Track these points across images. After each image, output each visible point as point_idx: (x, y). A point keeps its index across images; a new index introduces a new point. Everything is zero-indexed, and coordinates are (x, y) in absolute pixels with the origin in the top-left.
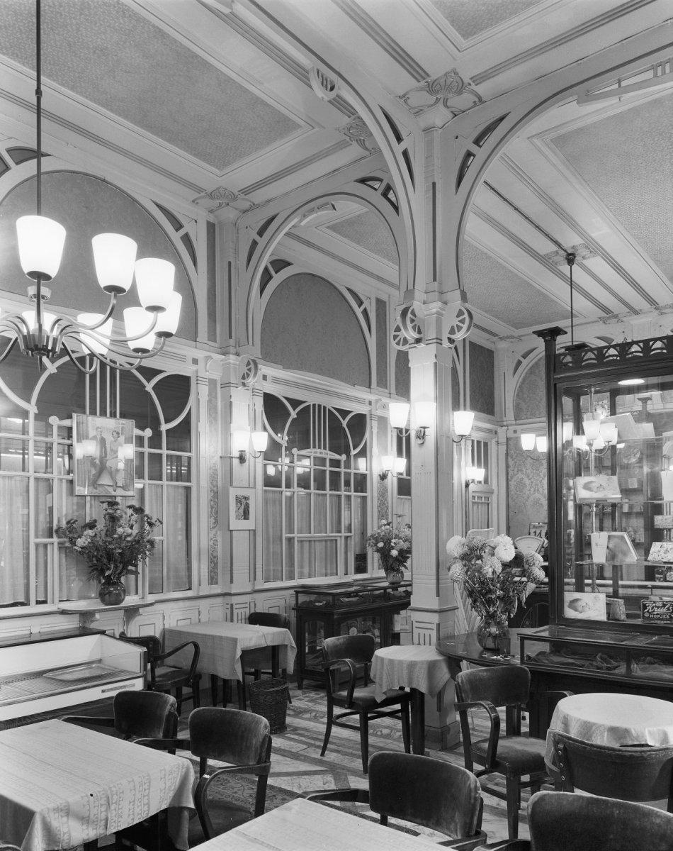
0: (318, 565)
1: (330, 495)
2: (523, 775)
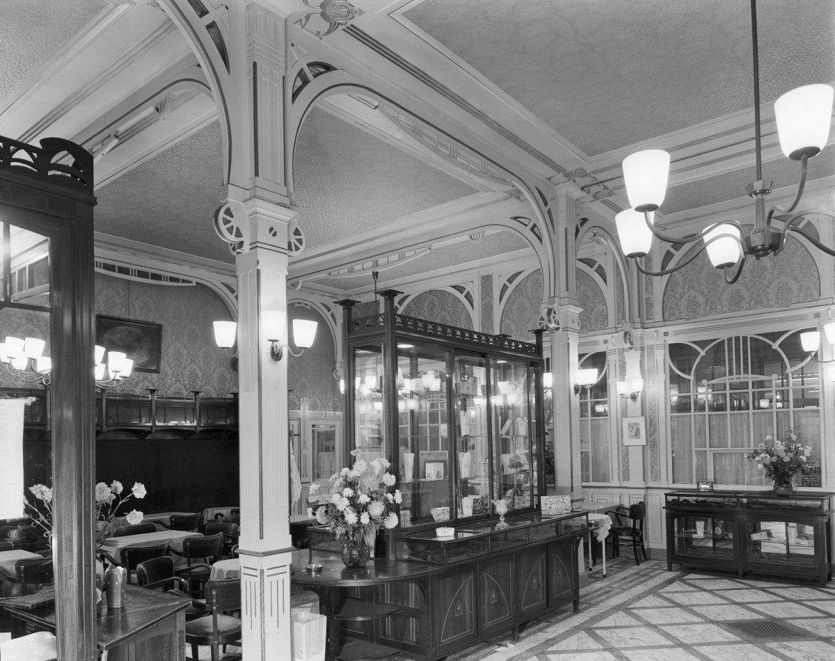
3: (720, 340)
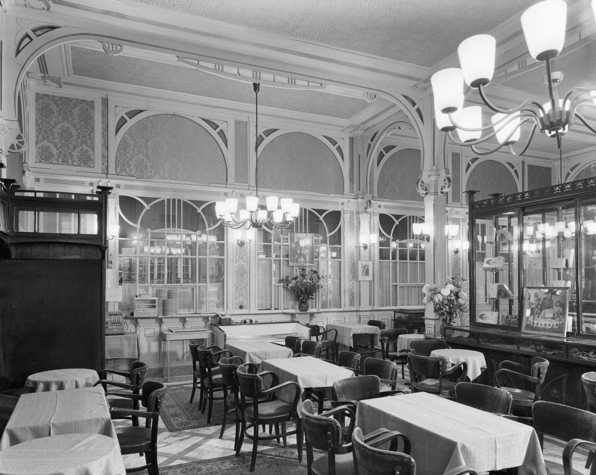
1: (399, 262)
2: (41, 197)
3: (404, 217)
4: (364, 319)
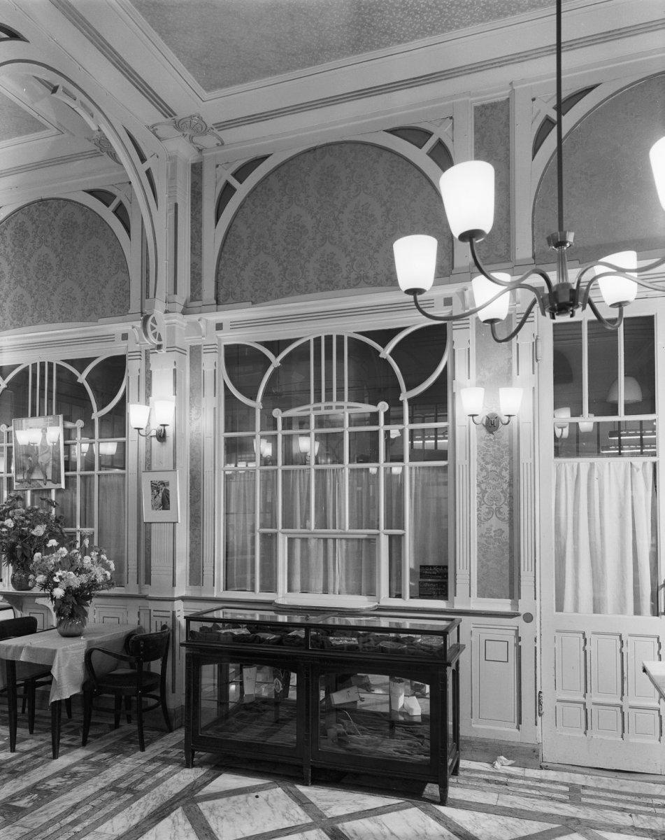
0: (338, 576)
4: (159, 620)
